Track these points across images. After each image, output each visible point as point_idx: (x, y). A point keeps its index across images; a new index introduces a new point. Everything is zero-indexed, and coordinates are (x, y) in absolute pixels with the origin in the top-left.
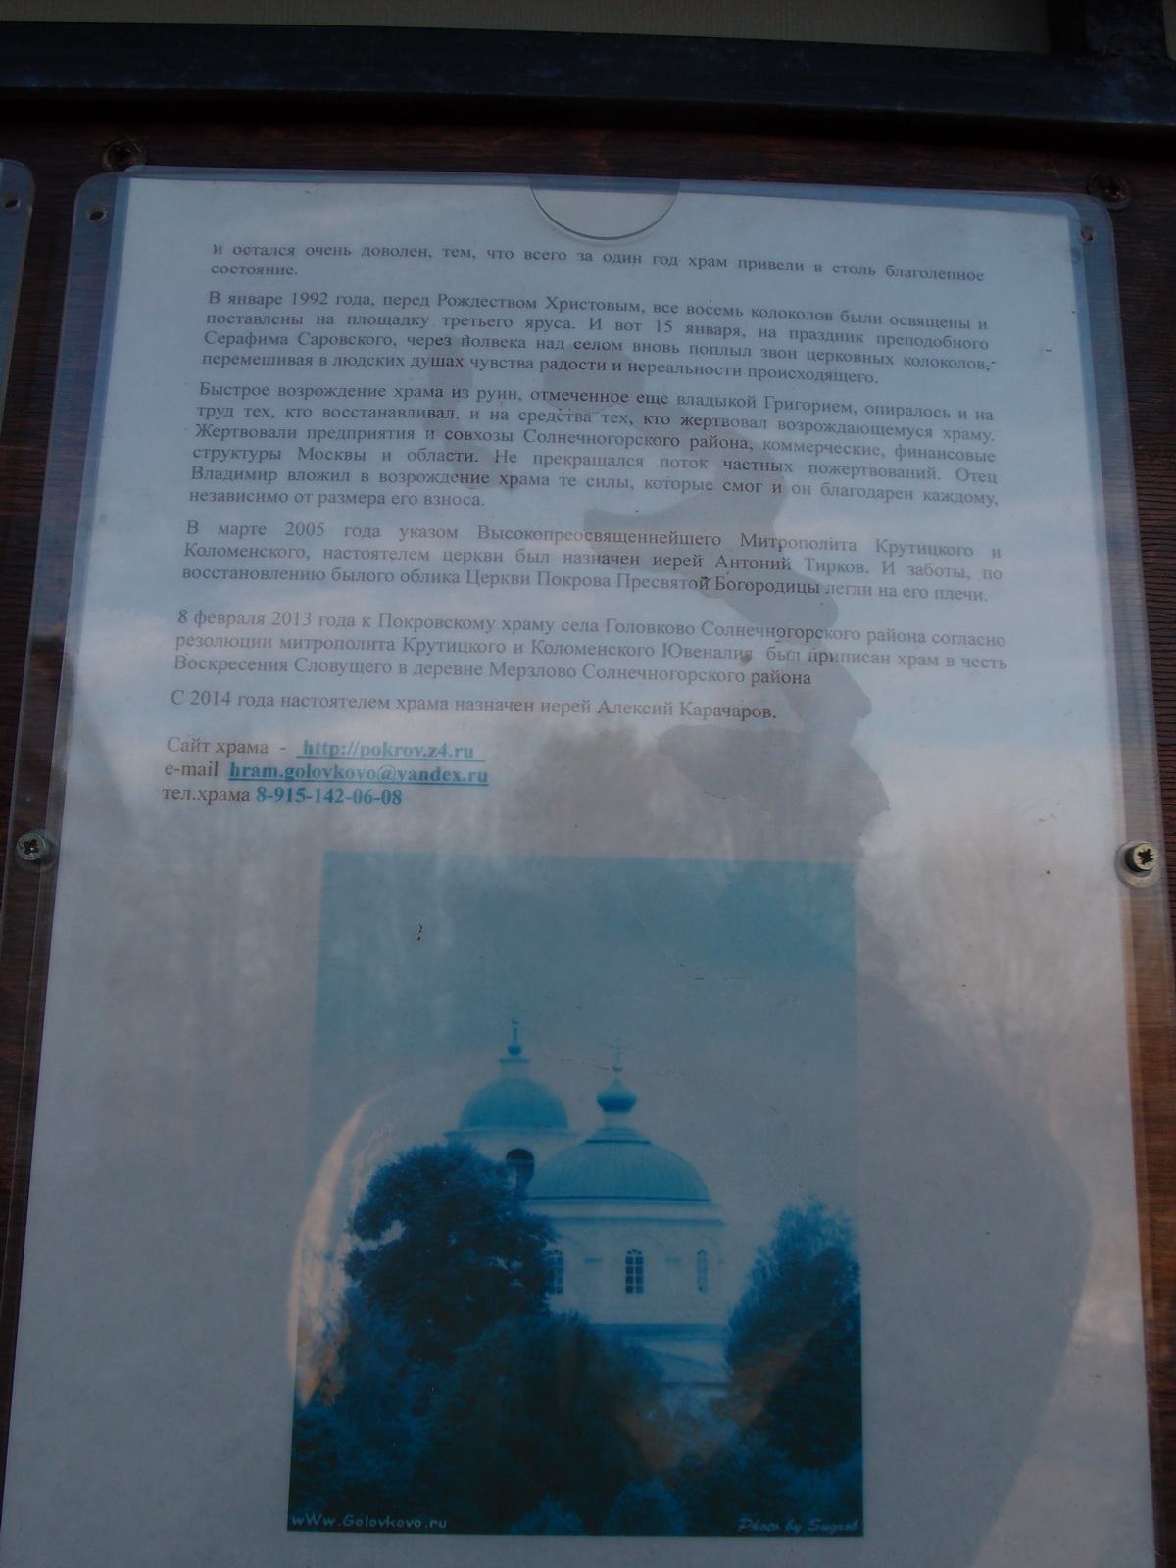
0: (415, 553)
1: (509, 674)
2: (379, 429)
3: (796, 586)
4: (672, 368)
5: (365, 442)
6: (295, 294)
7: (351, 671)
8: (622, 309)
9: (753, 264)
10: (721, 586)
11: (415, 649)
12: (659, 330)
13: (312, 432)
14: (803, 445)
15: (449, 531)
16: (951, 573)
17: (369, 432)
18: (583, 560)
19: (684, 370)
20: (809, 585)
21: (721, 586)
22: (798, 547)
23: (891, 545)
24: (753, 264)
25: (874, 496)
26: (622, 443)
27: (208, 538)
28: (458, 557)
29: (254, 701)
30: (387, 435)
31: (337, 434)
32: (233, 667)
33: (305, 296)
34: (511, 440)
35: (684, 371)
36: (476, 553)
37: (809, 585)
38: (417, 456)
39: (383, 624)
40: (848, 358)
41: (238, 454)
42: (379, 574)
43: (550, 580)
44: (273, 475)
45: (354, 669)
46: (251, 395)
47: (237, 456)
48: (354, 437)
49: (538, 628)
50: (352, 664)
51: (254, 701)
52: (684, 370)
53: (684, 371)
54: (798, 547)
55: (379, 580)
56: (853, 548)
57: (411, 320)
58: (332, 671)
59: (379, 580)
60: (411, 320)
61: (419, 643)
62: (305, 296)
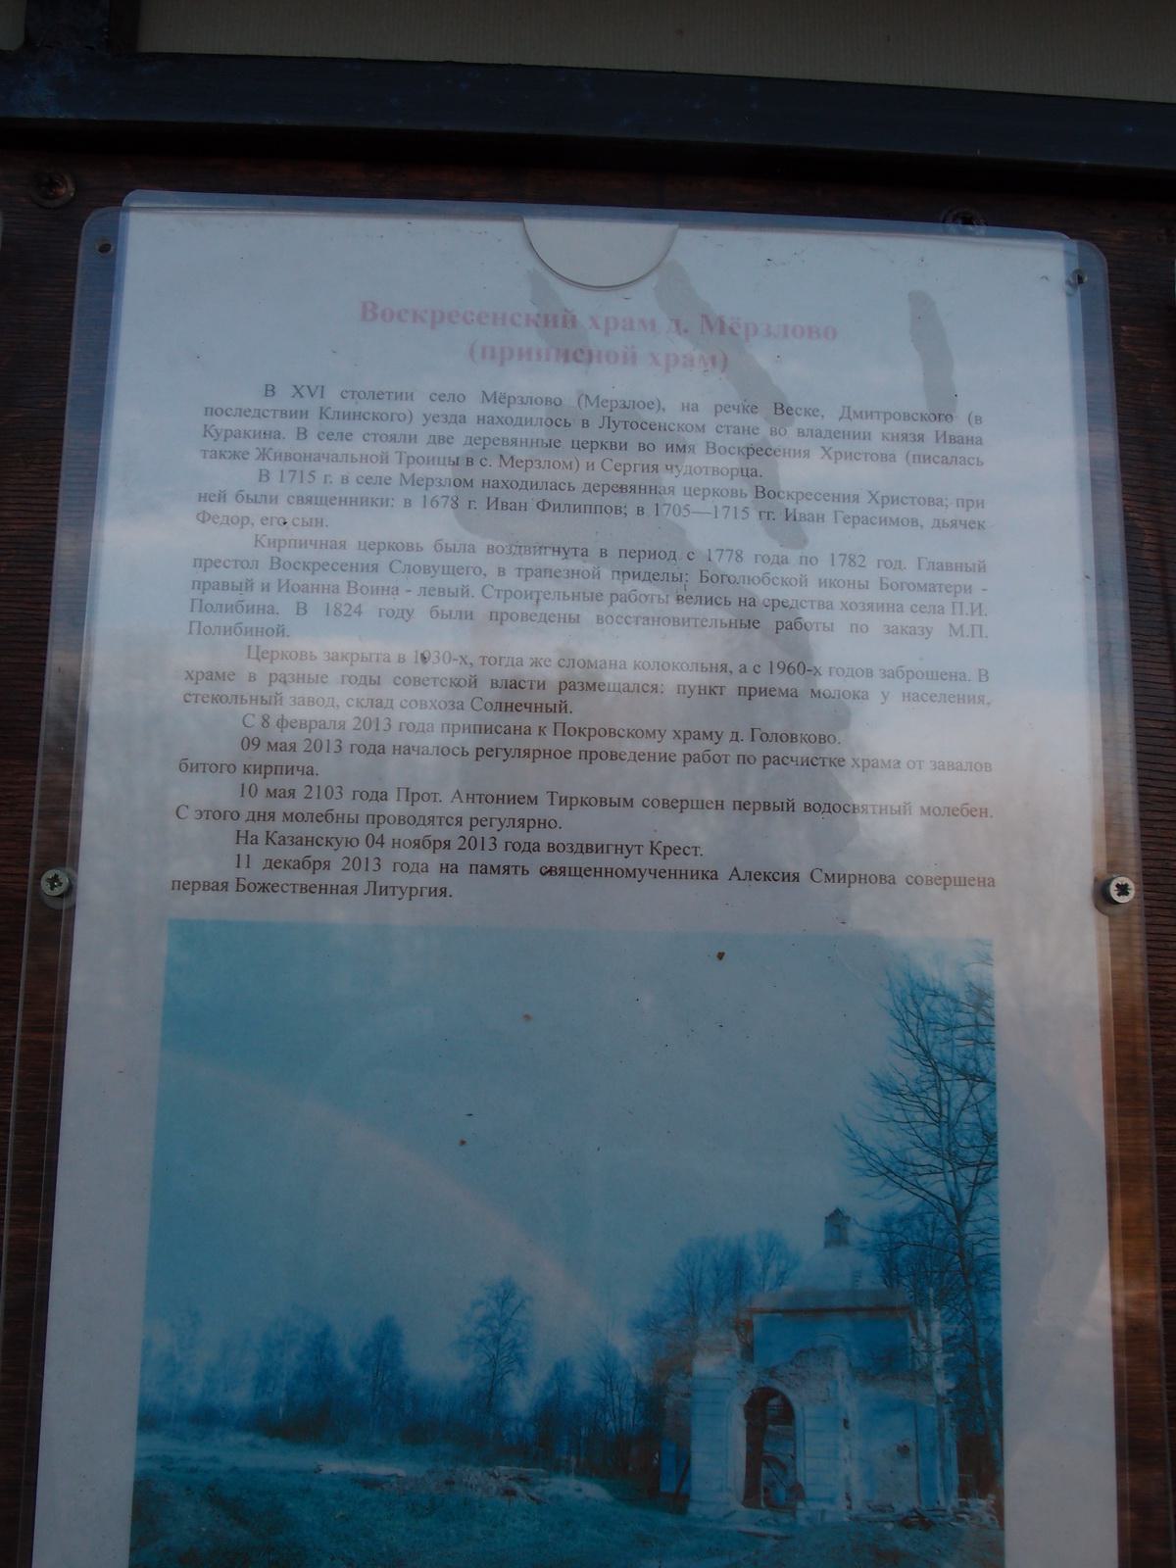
1: (519, 802)
3: (483, 731)
4: (324, 724)
6: (771, 663)
7: (443, 573)
9: (531, 824)
11: (662, 852)
12: (920, 568)
13: (742, 689)
15: (647, 731)
16: (821, 627)
17: (760, 688)
18: (577, 686)
19: (349, 459)
20: (547, 705)
21: (704, 579)
22: (661, 664)
24: (531, 824)
25: (374, 753)
26: (293, 585)
28: (372, 547)
32: (218, 565)
35: (670, 579)
36: (389, 543)
37: (547, 705)
39: (284, 479)
41: (715, 690)
43: (566, 731)
45: (446, 572)
47: (715, 693)
49: (680, 451)
52: (349, 459)
53: (670, 579)
54: (661, 664)
58: (425, 573)
61: (665, 847)
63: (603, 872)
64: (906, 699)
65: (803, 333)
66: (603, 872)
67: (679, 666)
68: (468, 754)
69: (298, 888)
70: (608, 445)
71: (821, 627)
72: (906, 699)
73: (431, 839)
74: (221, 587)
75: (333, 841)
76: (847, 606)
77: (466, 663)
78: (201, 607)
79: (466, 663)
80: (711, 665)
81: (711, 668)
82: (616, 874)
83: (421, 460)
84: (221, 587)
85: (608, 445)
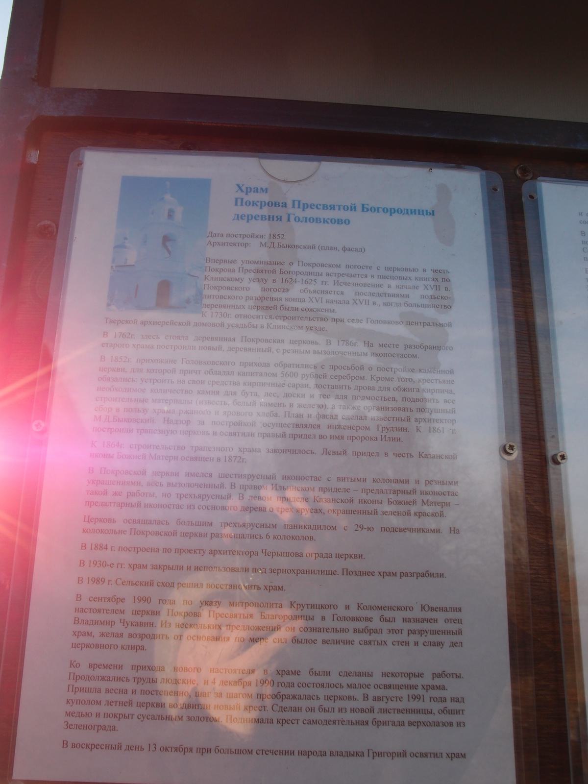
0: (101, 665)
2: (396, 293)
5: (145, 640)
8: (430, 214)
10: (282, 273)
14: (381, 607)
21: (282, 273)
23: (247, 188)
26: (350, 572)
27: (84, 670)
29: (84, 678)
30: (102, 611)
31: (76, 714)
33: (139, 599)
34: (313, 620)
38: (209, 372)
40: (381, 355)
42: (111, 645)
44: (113, 623)
46: (260, 342)
48: (243, 488)
50: (77, 700)
51: (84, 678)
55: (111, 648)
56: (167, 523)
57: (158, 566)
59: (111, 648)
60: (158, 566)
62: (139, 599)
63: (446, 632)
64: (405, 621)
65: (250, 204)
66: (446, 632)
67: (290, 478)
68: (260, 589)
69: (232, 383)
70: (353, 556)
71: (148, 495)
72: (405, 621)
73: (350, 376)
74: (377, 699)
75: (70, 701)
76: (165, 584)
77: (321, 513)
78: (347, 573)
79: (321, 513)
80: (166, 716)
81: (166, 718)
82: (371, 501)
83: (289, 318)
84: (377, 699)
85: (353, 556)
